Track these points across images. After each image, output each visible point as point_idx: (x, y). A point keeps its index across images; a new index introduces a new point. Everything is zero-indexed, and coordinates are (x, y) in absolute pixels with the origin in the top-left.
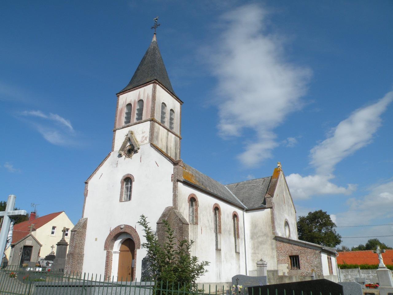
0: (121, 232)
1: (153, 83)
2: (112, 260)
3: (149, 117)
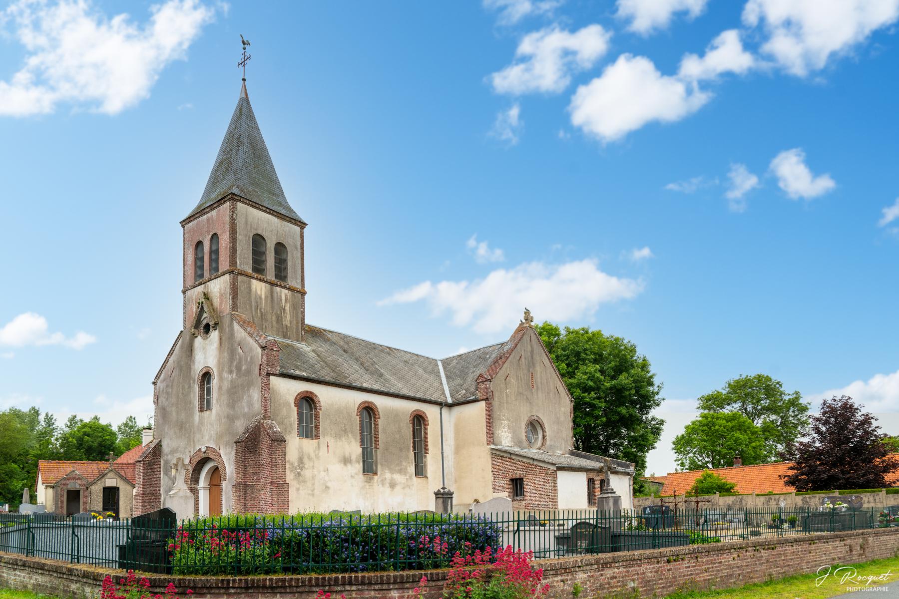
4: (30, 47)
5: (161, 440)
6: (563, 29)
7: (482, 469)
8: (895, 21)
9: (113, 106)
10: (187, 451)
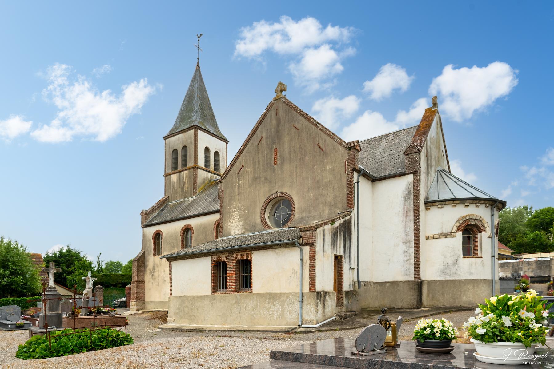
4: (60, 107)
6: (335, 98)
8: (508, 93)
9: (103, 137)
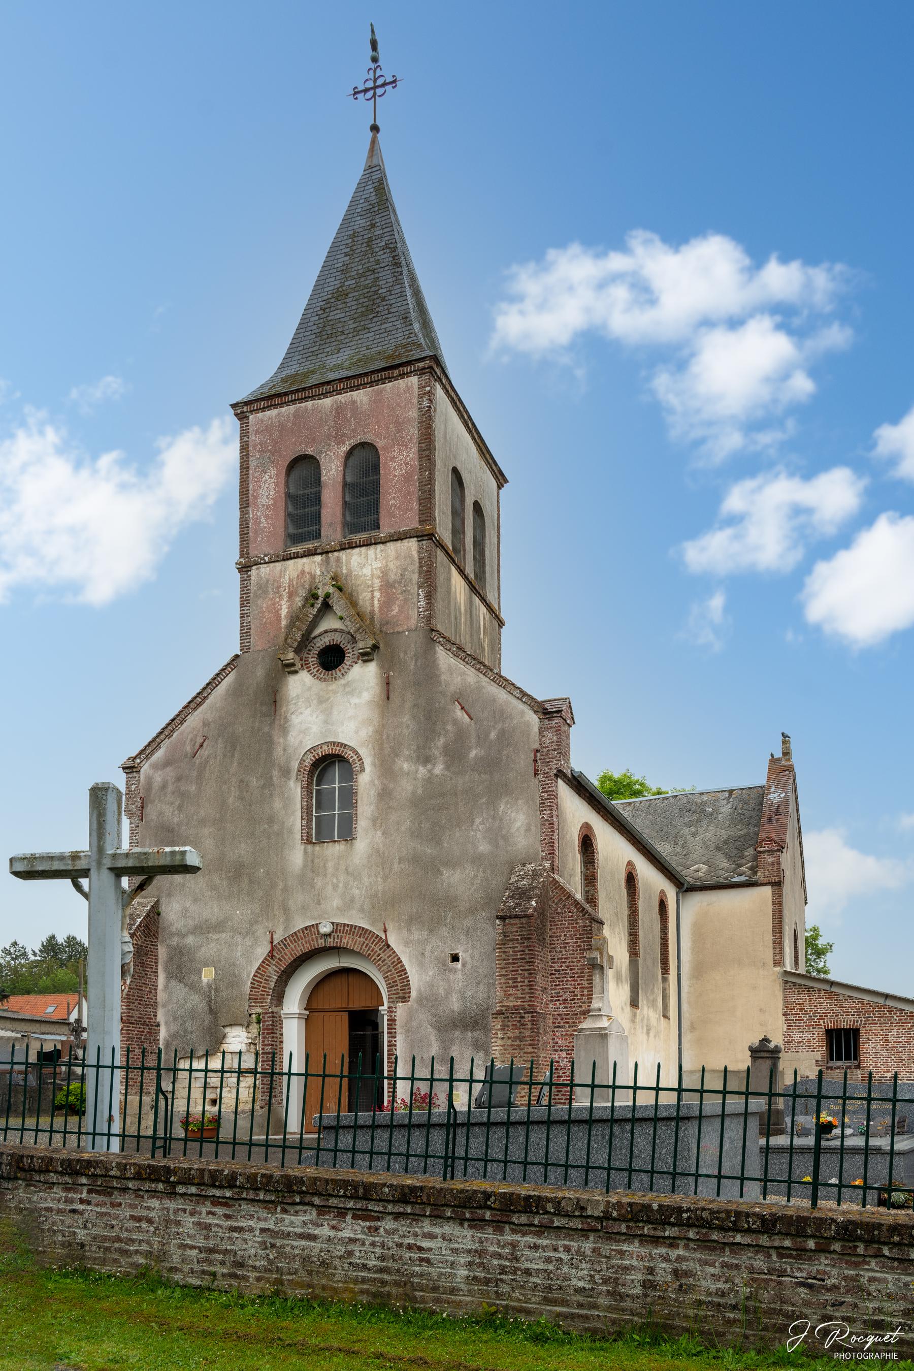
0: (316, 949)
1: (421, 372)
2: (282, 1042)
3: (412, 522)
5: (158, 901)
7: (761, 1010)
10: (261, 931)
